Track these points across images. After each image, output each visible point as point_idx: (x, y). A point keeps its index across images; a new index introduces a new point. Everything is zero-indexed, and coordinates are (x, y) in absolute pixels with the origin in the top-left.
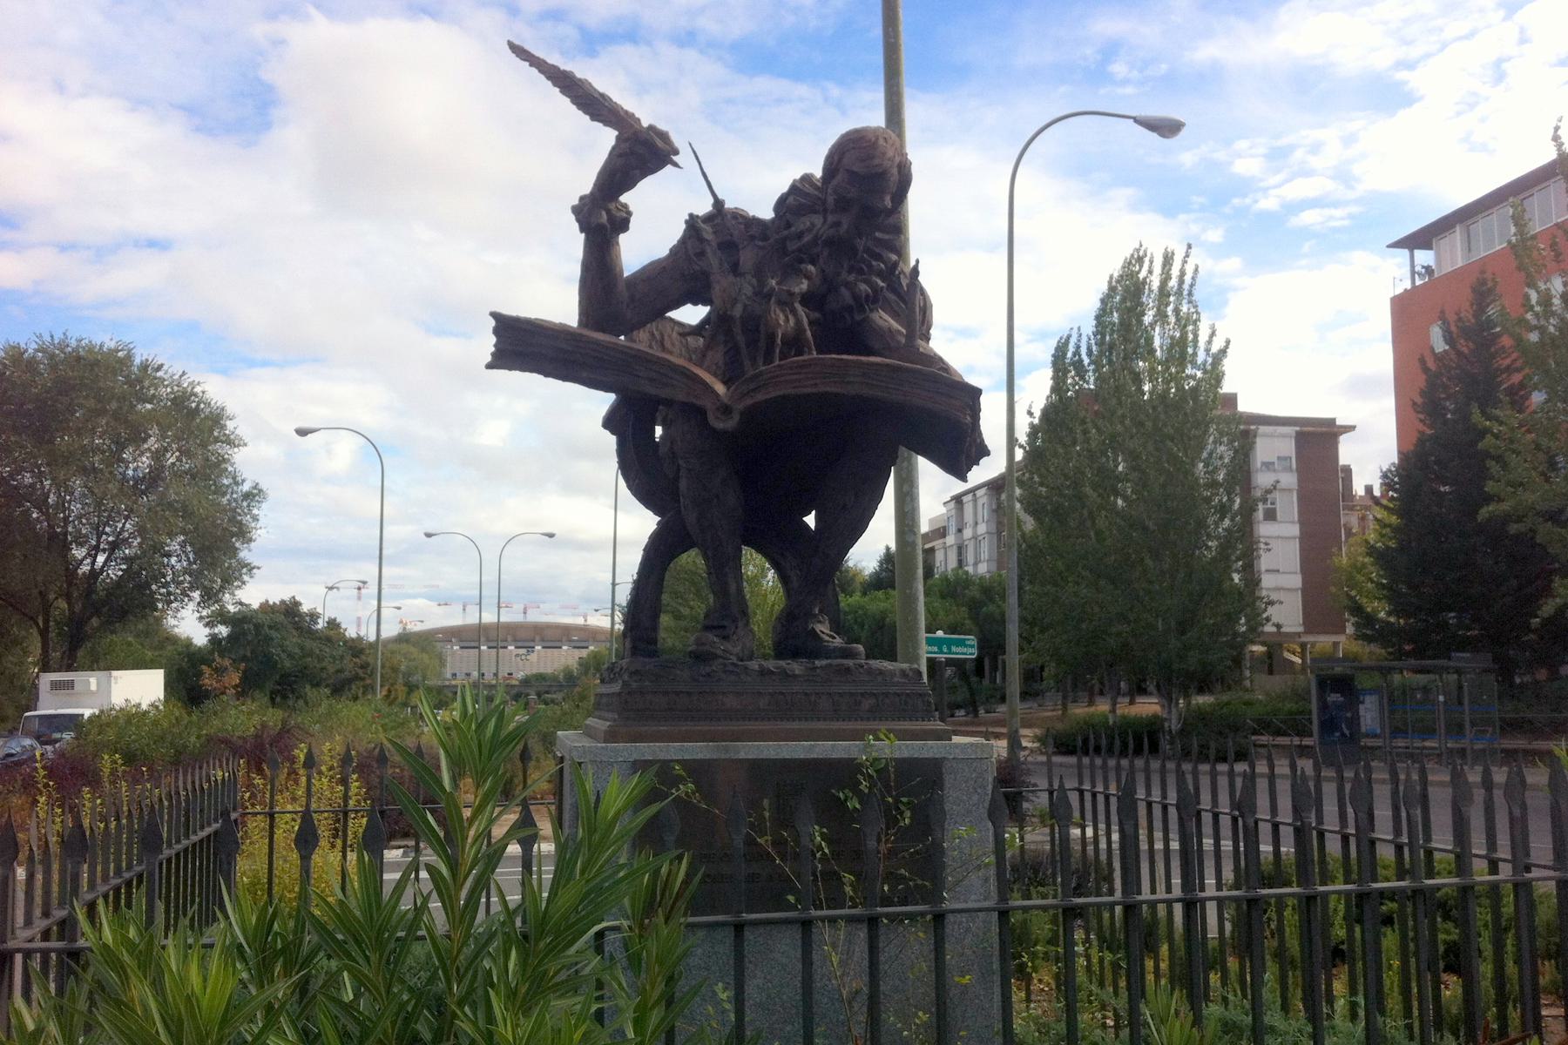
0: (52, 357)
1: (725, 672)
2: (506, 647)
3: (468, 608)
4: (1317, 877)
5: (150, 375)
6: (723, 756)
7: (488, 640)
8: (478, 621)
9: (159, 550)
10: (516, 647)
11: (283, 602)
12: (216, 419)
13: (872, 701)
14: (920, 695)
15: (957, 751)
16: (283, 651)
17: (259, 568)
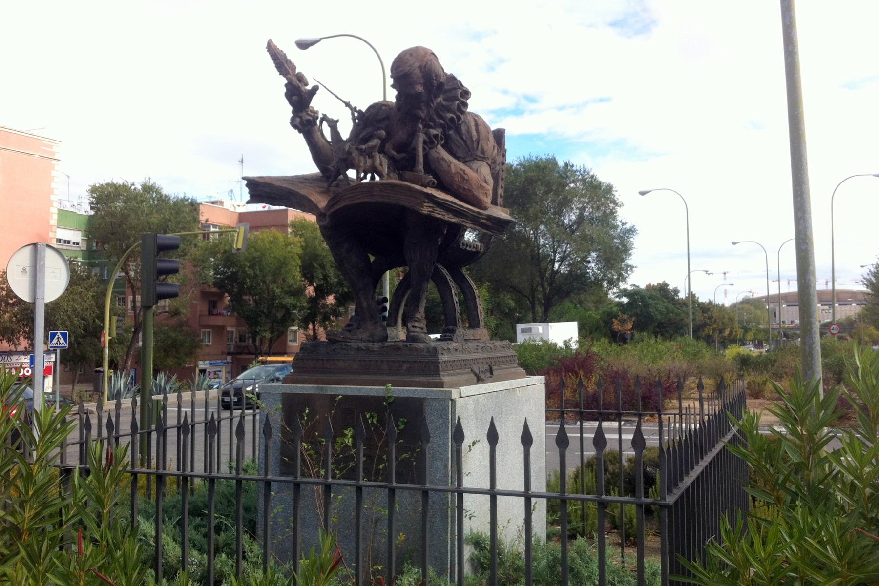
0: (524, 167)
1: (342, 349)
2: (851, 305)
3: (790, 282)
4: (642, 494)
5: (570, 170)
6: (321, 393)
7: (838, 300)
8: (767, 294)
9: (584, 259)
10: (822, 305)
11: (659, 284)
12: (609, 189)
13: (409, 365)
14: (433, 362)
15: (433, 394)
16: (657, 310)
17: (636, 267)
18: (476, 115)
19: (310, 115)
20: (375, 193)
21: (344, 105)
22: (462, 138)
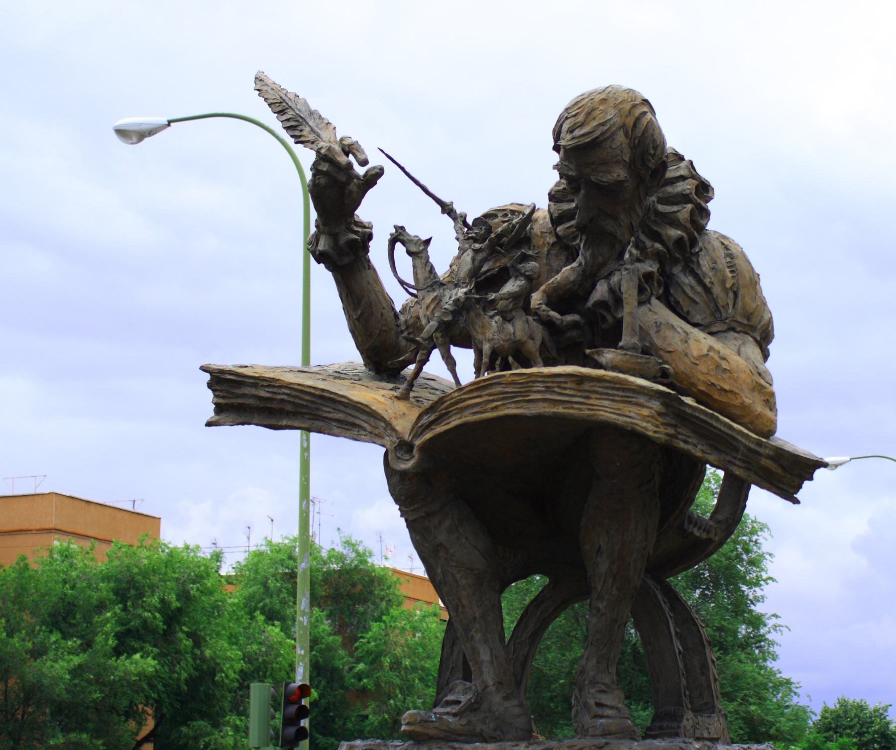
18: (724, 237)
19: (356, 233)
20: (533, 396)
21: (439, 208)
22: (700, 282)
